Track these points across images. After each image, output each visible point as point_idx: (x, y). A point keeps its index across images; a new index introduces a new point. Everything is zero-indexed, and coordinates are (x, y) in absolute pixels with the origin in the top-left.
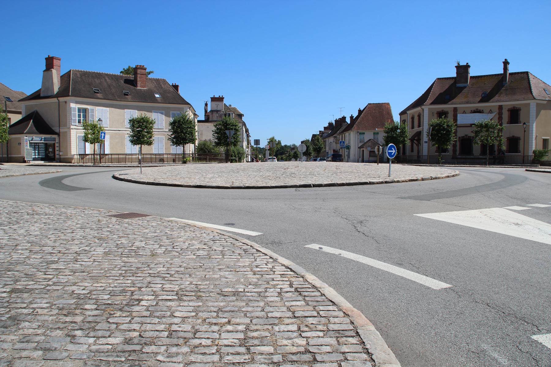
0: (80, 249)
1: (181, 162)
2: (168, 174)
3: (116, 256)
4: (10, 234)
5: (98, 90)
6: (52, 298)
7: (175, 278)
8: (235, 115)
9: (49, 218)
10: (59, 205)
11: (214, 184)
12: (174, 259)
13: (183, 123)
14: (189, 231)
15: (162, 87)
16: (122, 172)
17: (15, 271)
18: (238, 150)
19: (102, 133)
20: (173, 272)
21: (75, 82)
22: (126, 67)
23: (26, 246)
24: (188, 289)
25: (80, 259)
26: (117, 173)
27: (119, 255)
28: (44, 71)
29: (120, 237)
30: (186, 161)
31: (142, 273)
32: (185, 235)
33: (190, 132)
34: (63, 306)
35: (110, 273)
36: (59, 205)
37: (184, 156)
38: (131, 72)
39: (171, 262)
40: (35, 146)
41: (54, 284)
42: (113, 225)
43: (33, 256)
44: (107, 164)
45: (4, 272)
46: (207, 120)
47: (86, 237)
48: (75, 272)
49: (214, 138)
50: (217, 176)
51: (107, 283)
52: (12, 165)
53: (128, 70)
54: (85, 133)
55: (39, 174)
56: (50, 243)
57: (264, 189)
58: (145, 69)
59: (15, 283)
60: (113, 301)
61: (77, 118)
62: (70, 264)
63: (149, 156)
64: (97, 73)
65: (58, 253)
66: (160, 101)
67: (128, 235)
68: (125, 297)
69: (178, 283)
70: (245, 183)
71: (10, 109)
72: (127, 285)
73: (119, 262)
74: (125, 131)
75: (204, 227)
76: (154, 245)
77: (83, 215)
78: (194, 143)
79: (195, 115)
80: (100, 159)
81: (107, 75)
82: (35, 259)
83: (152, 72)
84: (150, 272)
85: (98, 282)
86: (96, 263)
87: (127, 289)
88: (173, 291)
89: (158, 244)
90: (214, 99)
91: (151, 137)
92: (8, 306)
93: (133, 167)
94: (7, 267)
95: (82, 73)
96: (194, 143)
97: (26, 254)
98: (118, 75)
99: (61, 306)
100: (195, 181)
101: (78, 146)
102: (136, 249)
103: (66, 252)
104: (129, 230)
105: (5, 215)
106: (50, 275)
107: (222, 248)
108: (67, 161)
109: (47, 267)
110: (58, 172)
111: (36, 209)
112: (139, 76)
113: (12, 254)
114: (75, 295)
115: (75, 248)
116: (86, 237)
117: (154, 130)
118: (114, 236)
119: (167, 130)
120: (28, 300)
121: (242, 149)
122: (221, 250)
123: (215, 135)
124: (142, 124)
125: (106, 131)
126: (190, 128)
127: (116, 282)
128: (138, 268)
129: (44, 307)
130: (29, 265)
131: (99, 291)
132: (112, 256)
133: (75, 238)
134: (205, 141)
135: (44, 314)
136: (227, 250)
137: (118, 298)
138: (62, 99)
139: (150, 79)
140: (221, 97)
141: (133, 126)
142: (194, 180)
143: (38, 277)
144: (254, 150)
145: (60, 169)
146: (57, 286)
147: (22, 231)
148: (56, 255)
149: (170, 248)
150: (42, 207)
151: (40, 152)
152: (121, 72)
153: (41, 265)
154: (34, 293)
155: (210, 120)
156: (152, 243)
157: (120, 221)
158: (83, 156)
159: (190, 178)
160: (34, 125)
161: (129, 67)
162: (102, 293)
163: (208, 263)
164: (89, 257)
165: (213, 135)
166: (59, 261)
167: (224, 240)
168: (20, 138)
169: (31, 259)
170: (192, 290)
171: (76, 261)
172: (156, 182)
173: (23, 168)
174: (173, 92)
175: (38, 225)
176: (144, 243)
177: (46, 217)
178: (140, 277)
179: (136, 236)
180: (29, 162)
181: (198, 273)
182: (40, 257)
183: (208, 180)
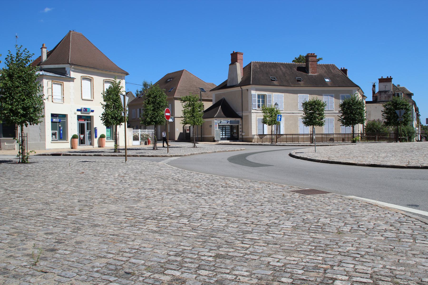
0: (271, 222)
1: (351, 142)
2: (341, 153)
3: (304, 231)
4: (210, 204)
5: (274, 78)
6: (251, 267)
7: (366, 259)
8: (404, 95)
9: (240, 191)
10: (247, 180)
11: (389, 164)
12: (362, 239)
13: (352, 105)
14: (371, 210)
15: (331, 72)
16: (298, 151)
17: (217, 238)
18: (408, 129)
19: (278, 116)
20: (363, 253)
21: (255, 72)
22: (298, 57)
23: (224, 215)
24: (382, 273)
25: (271, 231)
26: (293, 151)
27: (306, 230)
28: (230, 65)
29: (306, 213)
30: (356, 141)
31: (331, 250)
32: (368, 214)
33: (359, 113)
34: (262, 277)
35: (301, 247)
36: (247, 180)
37: (353, 136)
38: (302, 60)
39: (358, 241)
40: (222, 127)
41: (251, 253)
42: (297, 201)
43: (230, 225)
44: (282, 143)
45: (208, 237)
46: (375, 101)
47: (274, 211)
48: (268, 244)
49: (383, 118)
50: (390, 155)
51: (299, 257)
52: (205, 144)
53: (299, 58)
54: (264, 116)
55: (226, 151)
56: (244, 214)
57: (384, 168)
58: (316, 56)
59: (218, 249)
60: (307, 277)
61: (257, 104)
62: (263, 235)
63: (320, 136)
64: (273, 63)
65: (251, 224)
66: (330, 85)
67: (312, 211)
68: (318, 274)
69: (371, 265)
70: (422, 163)
71: (204, 97)
72: (318, 261)
73: (307, 237)
74: (298, 113)
75: (386, 207)
76: (339, 223)
77: (269, 190)
78: (363, 123)
79: (363, 96)
80: (277, 138)
81: (282, 64)
82: (232, 228)
83: (321, 59)
84: (339, 250)
85: (290, 256)
86: (286, 236)
87: (319, 266)
88: (367, 273)
89: (343, 222)
90: (382, 80)
91: (322, 119)
92: (214, 270)
93: (306, 146)
94: (210, 233)
95: (261, 64)
96: (363, 123)
97: (224, 223)
98: (291, 64)
99: (260, 276)
100: (369, 160)
101: (257, 128)
102: (322, 225)
103: (258, 223)
104: (313, 206)
105: (205, 186)
106: (246, 244)
107: (411, 231)
108: (248, 140)
109: (244, 237)
110: (242, 150)
111: (229, 182)
112: (310, 63)
113: (213, 222)
114: (271, 267)
115: (266, 220)
116: (274, 211)
117: (325, 112)
118: (300, 211)
119: (338, 112)
120: (231, 267)
121: (412, 128)
122: (410, 233)
123: (384, 115)
124: (314, 107)
125: (282, 114)
126: (359, 109)
127: (307, 257)
128: (327, 245)
129: (244, 275)
130: (228, 233)
131: (293, 265)
132: (301, 230)
133: (264, 211)
134: (374, 121)
135: (246, 282)
136: (417, 234)
137: (312, 274)
138: (244, 88)
139: (320, 65)
140: (389, 77)
141: (306, 109)
142: (367, 159)
143: (236, 245)
144: (424, 129)
145: (243, 148)
146: (254, 256)
147: (219, 202)
148: (250, 226)
149: (355, 227)
150: (233, 181)
151: (226, 133)
152: (293, 61)
153: (238, 234)
154: (235, 260)
155: (378, 100)
156: (337, 220)
157: (303, 196)
158: (262, 136)
159: (363, 157)
160: (222, 110)
161: (300, 56)
162: (295, 267)
163: (398, 247)
164: (279, 230)
165: (382, 115)
166: (253, 231)
167: (411, 222)
168: (211, 122)
169: (229, 228)
170: (387, 274)
171: (268, 233)
172: (330, 160)
173: (214, 147)
174: (342, 76)
175: (232, 197)
176: (329, 219)
177: (237, 190)
178: (330, 254)
179: (320, 213)
180: (217, 141)
181: (390, 257)
182: (236, 226)
183: (381, 159)
